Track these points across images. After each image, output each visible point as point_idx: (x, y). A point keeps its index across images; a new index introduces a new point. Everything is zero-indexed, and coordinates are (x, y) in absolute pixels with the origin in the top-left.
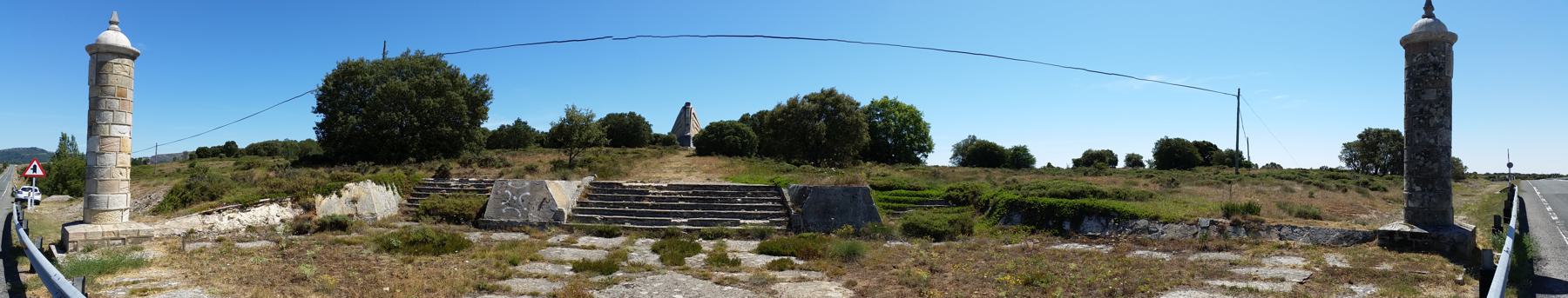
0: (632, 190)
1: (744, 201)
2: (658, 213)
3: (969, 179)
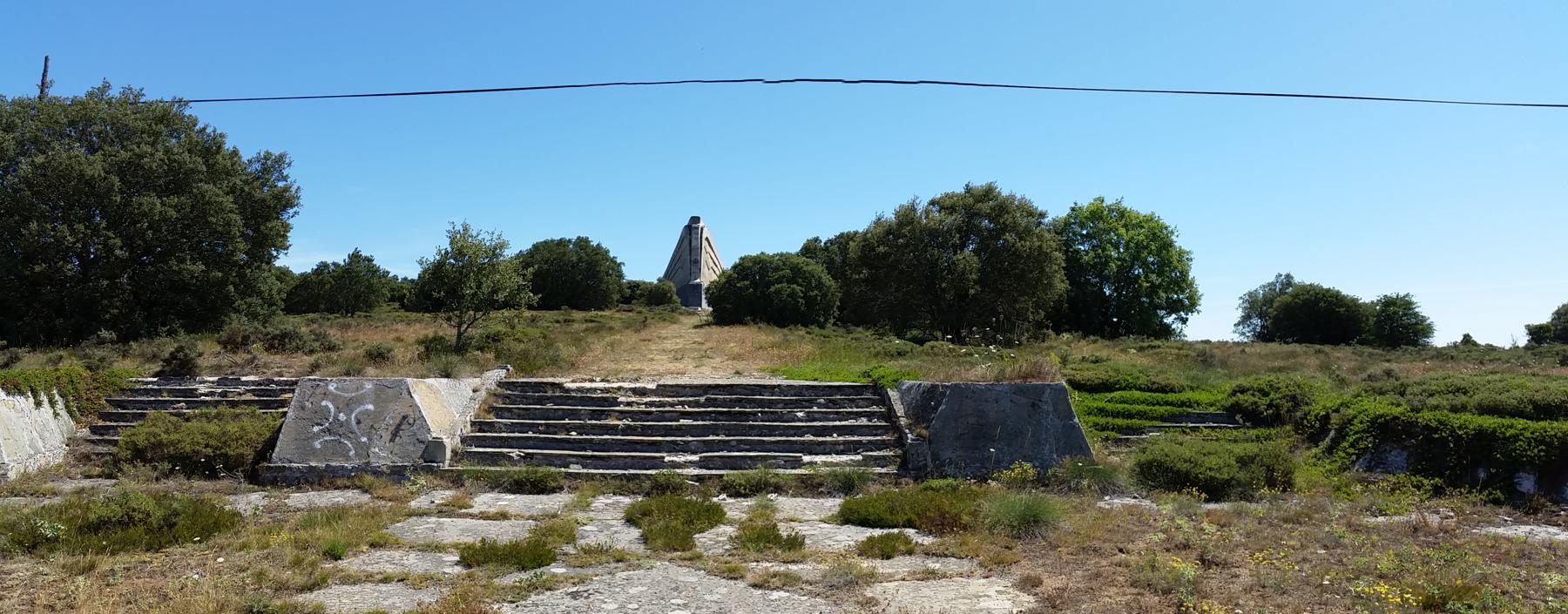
0: (585, 398)
1: (810, 417)
2: (642, 442)
3: (1280, 370)
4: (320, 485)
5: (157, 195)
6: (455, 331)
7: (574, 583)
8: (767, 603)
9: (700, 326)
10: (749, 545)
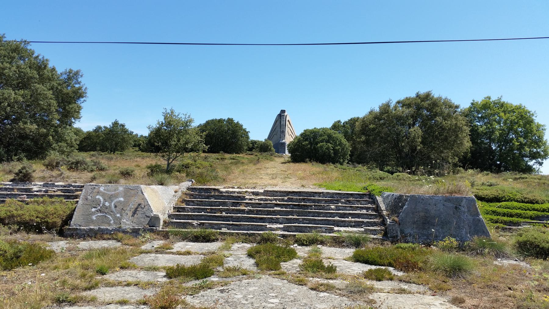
0: (229, 196)
1: (338, 208)
2: (254, 218)
4: (95, 238)
5: (12, 89)
6: (166, 162)
7: (222, 285)
8: (318, 298)
9: (285, 163)
10: (309, 269)
